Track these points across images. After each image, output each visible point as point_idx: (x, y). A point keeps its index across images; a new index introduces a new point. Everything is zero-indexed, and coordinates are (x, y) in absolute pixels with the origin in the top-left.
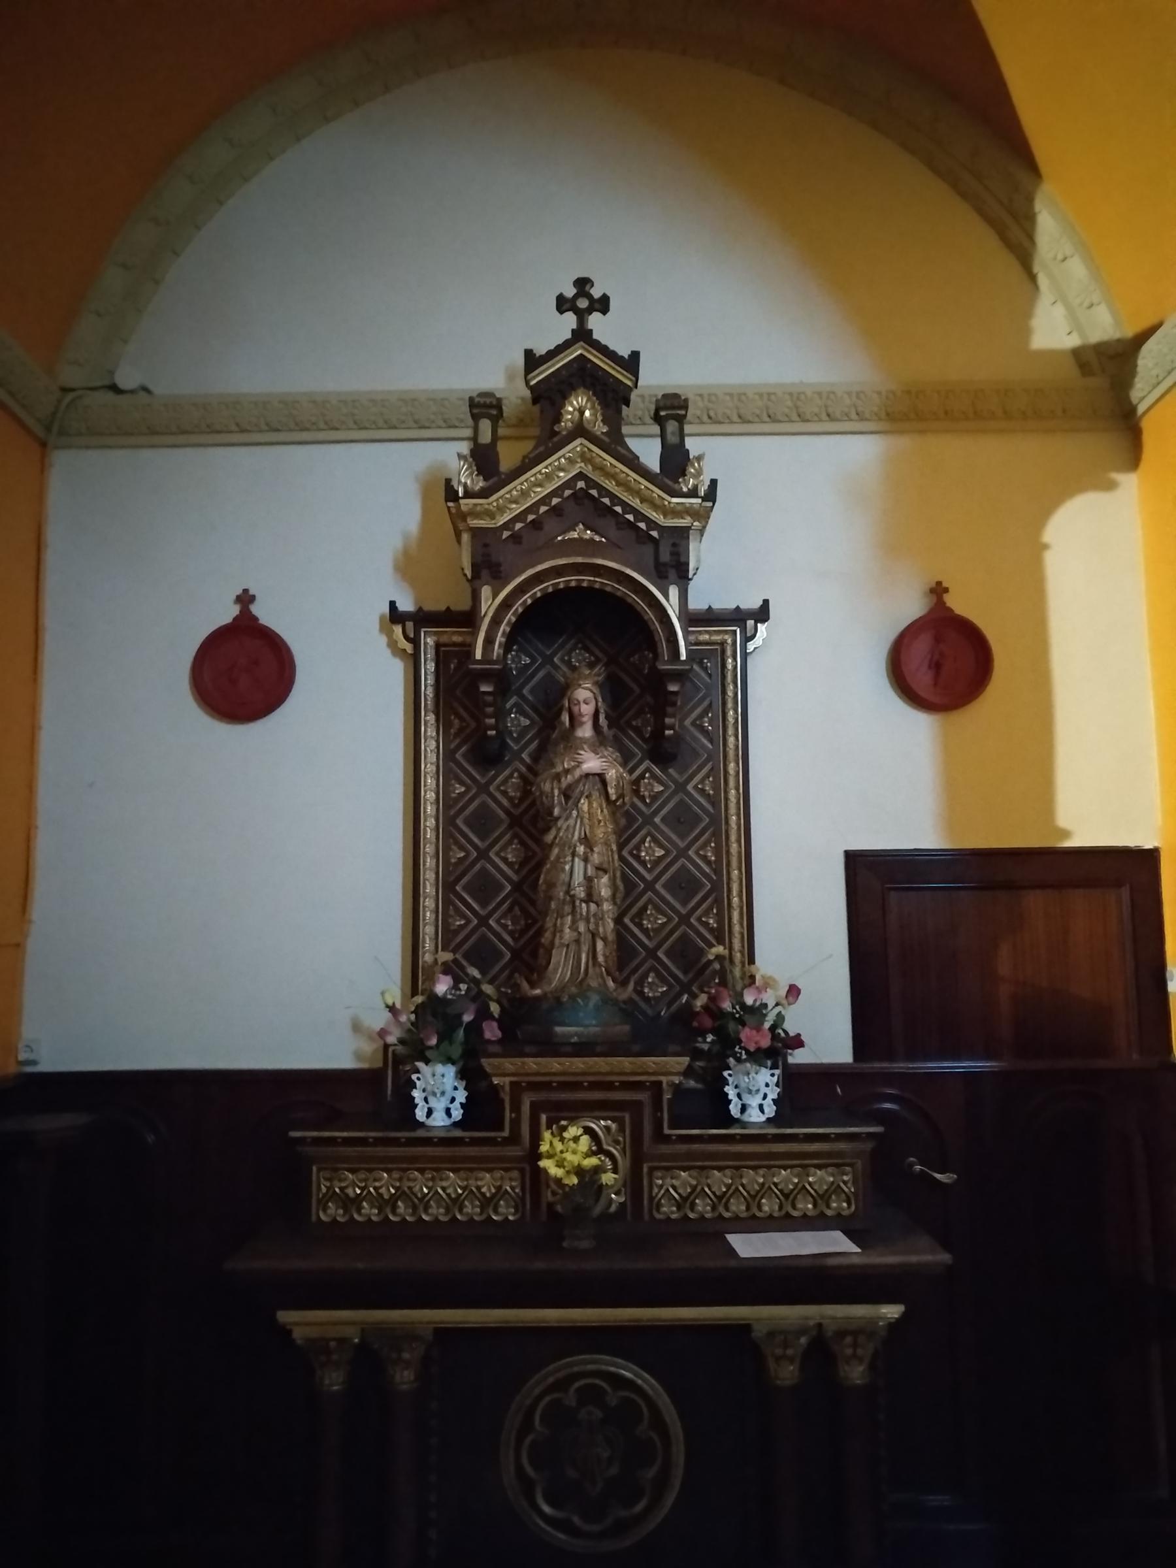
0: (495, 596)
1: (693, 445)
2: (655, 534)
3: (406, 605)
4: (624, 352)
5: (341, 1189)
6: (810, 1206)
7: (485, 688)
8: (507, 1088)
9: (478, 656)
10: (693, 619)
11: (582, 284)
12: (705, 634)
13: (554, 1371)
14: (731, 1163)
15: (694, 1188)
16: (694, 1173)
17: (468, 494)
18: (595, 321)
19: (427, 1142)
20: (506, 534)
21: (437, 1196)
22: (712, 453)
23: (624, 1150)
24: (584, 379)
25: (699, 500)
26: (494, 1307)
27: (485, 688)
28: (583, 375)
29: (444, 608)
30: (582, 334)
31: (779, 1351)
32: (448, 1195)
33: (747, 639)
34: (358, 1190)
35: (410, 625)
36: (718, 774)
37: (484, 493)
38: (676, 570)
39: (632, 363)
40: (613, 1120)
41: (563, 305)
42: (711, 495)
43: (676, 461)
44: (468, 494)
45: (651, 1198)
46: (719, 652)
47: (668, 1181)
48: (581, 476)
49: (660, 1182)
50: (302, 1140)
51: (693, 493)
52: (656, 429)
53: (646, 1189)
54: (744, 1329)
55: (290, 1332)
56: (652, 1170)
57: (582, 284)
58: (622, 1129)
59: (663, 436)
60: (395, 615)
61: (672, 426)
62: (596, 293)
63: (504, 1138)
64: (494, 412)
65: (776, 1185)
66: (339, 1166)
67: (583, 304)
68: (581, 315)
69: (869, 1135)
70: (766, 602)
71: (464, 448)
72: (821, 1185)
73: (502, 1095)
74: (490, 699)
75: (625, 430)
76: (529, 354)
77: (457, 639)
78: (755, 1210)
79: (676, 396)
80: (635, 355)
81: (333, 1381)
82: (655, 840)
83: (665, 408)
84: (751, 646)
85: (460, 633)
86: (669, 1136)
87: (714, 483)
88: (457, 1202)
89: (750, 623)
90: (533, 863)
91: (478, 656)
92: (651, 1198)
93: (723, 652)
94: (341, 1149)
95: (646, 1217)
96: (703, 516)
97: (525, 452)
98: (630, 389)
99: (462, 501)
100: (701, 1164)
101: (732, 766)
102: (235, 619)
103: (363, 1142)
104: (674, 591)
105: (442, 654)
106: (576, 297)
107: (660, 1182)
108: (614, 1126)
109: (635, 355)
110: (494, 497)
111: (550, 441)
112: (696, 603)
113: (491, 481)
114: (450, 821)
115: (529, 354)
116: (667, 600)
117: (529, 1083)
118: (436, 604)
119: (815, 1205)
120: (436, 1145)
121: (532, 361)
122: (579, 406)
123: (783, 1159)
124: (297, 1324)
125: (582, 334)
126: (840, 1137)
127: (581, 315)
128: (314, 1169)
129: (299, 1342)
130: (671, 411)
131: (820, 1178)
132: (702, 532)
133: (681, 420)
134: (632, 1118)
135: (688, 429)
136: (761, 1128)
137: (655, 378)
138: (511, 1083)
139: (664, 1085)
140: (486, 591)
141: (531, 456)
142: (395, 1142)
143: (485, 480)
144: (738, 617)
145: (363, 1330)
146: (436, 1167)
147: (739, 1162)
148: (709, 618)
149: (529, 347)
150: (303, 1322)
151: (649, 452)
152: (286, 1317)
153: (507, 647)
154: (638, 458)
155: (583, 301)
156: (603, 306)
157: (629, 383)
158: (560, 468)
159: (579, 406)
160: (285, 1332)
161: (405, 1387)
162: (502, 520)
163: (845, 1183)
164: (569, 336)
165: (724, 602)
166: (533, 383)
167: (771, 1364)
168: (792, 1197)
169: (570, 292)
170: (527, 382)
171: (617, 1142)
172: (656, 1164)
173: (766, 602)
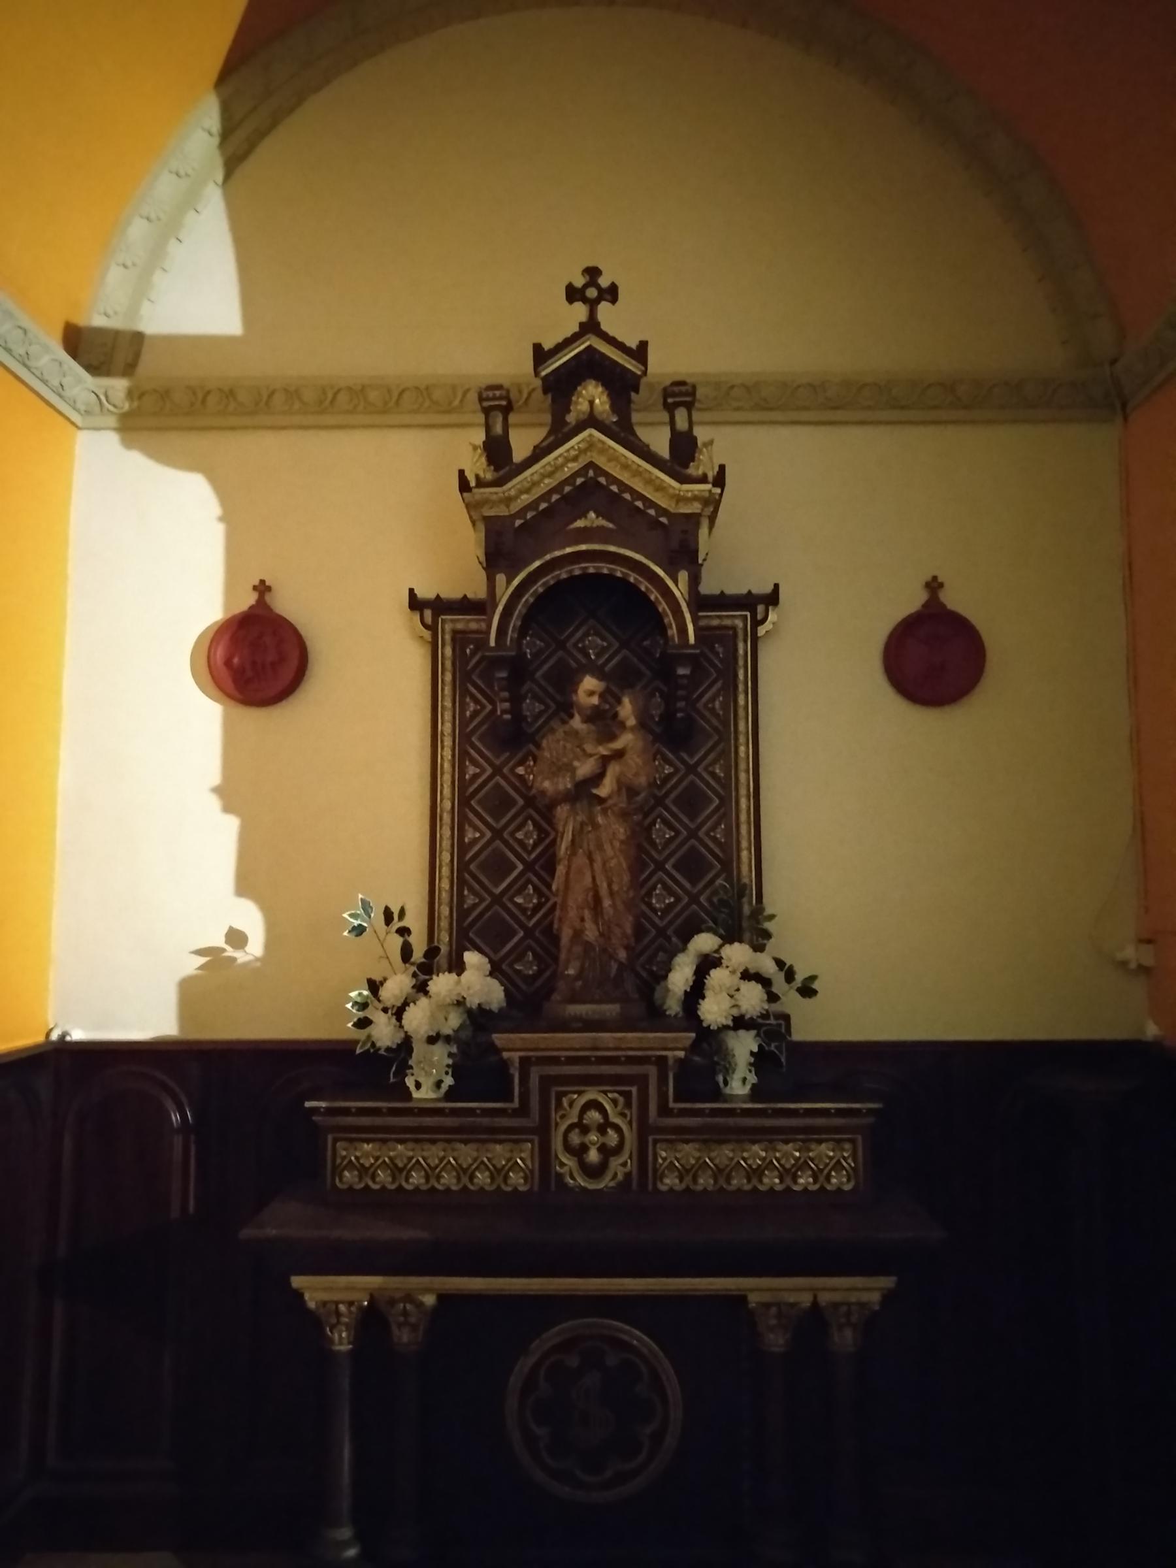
0: (509, 582)
1: (701, 434)
2: (663, 520)
3: (423, 593)
4: (632, 344)
5: (357, 1158)
6: (777, 1181)
7: (682, 671)
8: (517, 1060)
9: (492, 643)
10: (700, 603)
11: (593, 273)
12: (714, 618)
13: (553, 1335)
14: (443, 1136)
15: (475, 1160)
16: (410, 1145)
17: (481, 483)
18: (604, 311)
19: (731, 1112)
20: (518, 523)
21: (771, 1166)
22: (719, 442)
23: (630, 1123)
24: (589, 372)
25: (708, 486)
26: (559, 1276)
27: (682, 671)
28: (591, 366)
29: (718, 592)
30: (591, 326)
31: (843, 1320)
32: (750, 1166)
33: (757, 623)
34: (366, 1160)
35: (428, 614)
36: (727, 756)
37: (498, 483)
38: (684, 554)
39: (640, 353)
40: (621, 1093)
41: (573, 295)
42: (720, 480)
43: (684, 448)
44: (481, 483)
45: (655, 1170)
46: (728, 637)
47: (771, 1153)
48: (591, 465)
49: (344, 1153)
50: (315, 1110)
51: (703, 479)
52: (665, 416)
53: (650, 1158)
54: (739, 1300)
55: (301, 1295)
56: (655, 1142)
57: (593, 273)
58: (628, 1104)
59: (672, 422)
60: (415, 603)
61: (681, 416)
62: (604, 282)
63: (514, 1110)
64: (670, 400)
65: (812, 1160)
66: (775, 1137)
67: (592, 293)
68: (593, 304)
69: (870, 1110)
70: (776, 586)
71: (479, 437)
72: (788, 1160)
73: (512, 1071)
74: (685, 681)
75: (636, 417)
76: (537, 348)
77: (473, 626)
78: (433, 1182)
79: (682, 383)
80: (643, 345)
81: (341, 1341)
82: (665, 822)
83: (674, 395)
84: (761, 630)
85: (478, 621)
86: (672, 1109)
87: (722, 468)
88: (758, 1173)
89: (760, 608)
90: (547, 841)
91: (492, 643)
92: (334, 1167)
93: (735, 635)
94: (479, 1120)
95: (650, 1187)
96: (714, 503)
97: (536, 442)
98: (639, 378)
99: (475, 491)
100: (382, 1135)
101: (742, 749)
102: (251, 607)
103: (376, 1112)
104: (683, 576)
105: (460, 639)
106: (586, 286)
107: (344, 1153)
108: (621, 1100)
109: (643, 345)
110: (509, 485)
111: (560, 433)
112: (708, 587)
113: (502, 473)
114: (724, 801)
115: (537, 348)
116: (677, 585)
117: (538, 1058)
118: (451, 593)
119: (781, 1181)
120: (446, 1115)
121: (540, 355)
122: (593, 396)
123: (399, 1133)
124: (752, 1290)
125: (591, 326)
126: (840, 1113)
127: (593, 304)
128: (330, 1138)
129: (312, 1305)
130: (680, 396)
131: (826, 1150)
132: (712, 519)
133: (689, 406)
134: (639, 1090)
135: (696, 416)
136: (745, 1102)
137: (663, 365)
138: (521, 1058)
139: (671, 1062)
140: (501, 578)
141: (544, 444)
142: (346, 1112)
143: (496, 470)
144: (748, 602)
145: (372, 1296)
146: (418, 1135)
147: (712, 1136)
148: (722, 602)
149: (536, 341)
150: (314, 1289)
151: (659, 441)
152: (297, 1281)
153: (523, 631)
154: (648, 446)
155: (592, 290)
156: (611, 294)
157: (639, 373)
158: (566, 459)
159: (593, 396)
160: (298, 1295)
161: (776, 1349)
162: (515, 507)
163: (845, 1158)
164: (577, 329)
165: (736, 588)
166: (543, 373)
167: (394, 1329)
168: (503, 1173)
169: (579, 282)
170: (537, 374)
171: (623, 1115)
172: (658, 1137)
173: (776, 586)
